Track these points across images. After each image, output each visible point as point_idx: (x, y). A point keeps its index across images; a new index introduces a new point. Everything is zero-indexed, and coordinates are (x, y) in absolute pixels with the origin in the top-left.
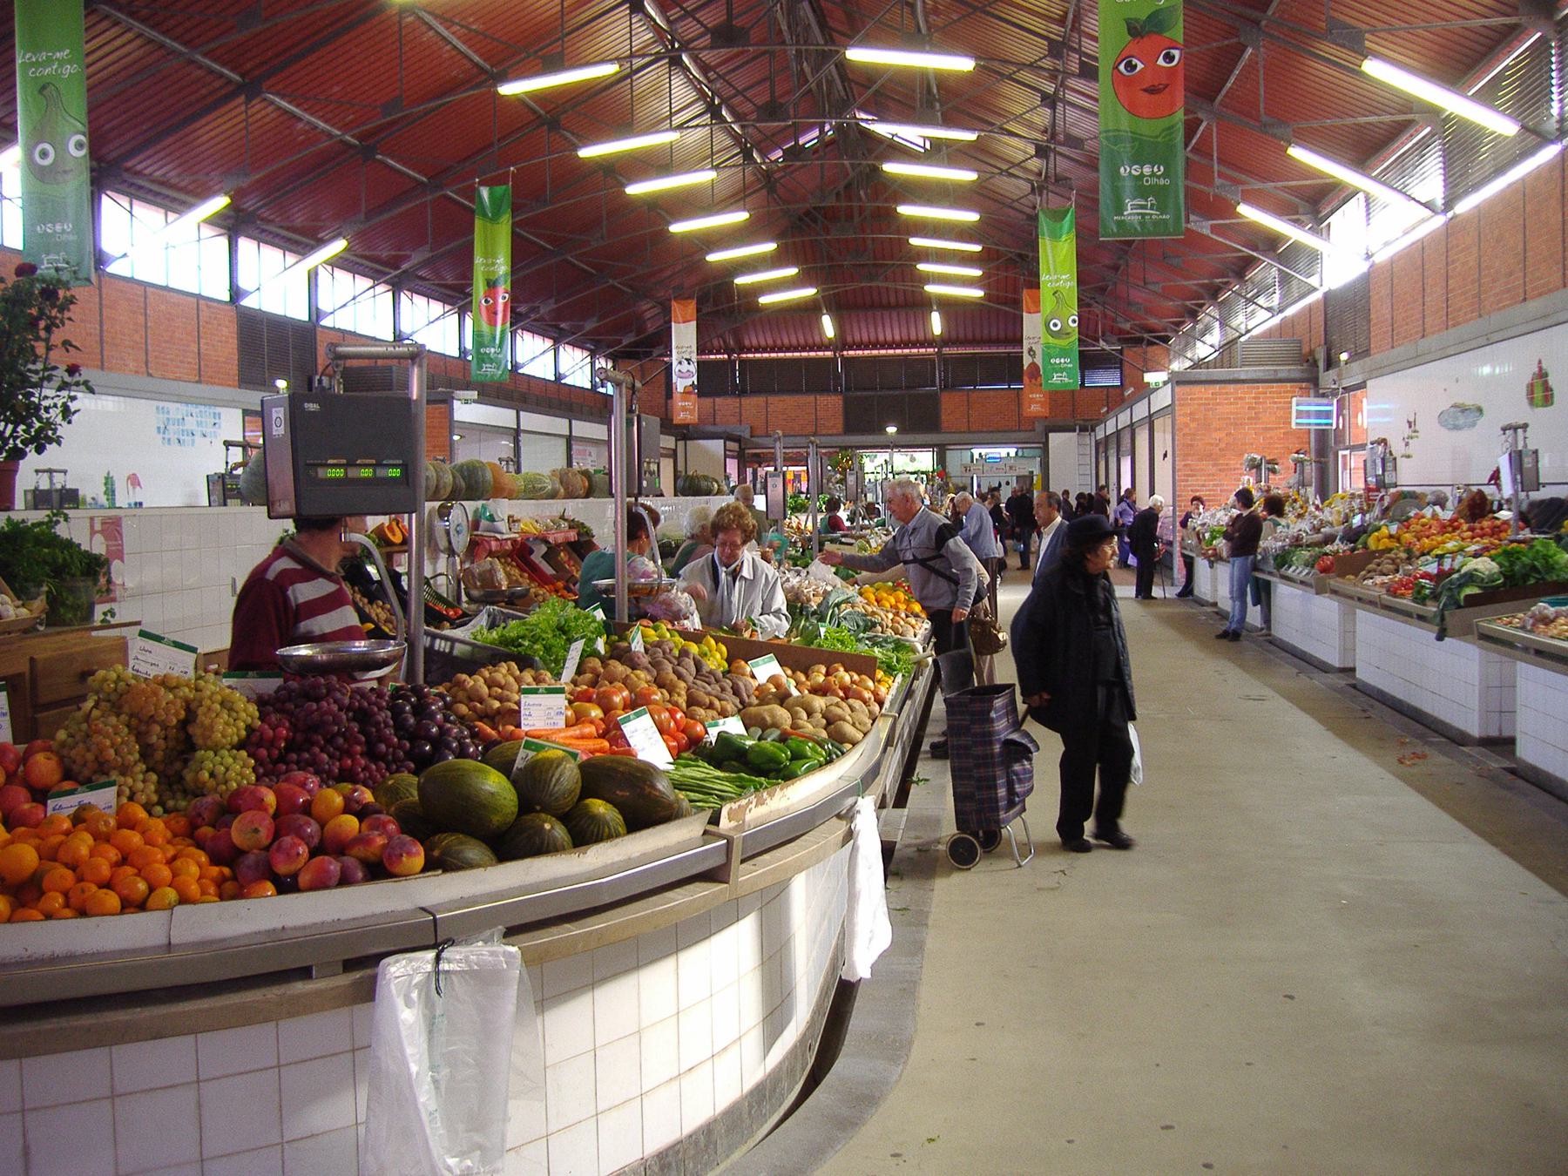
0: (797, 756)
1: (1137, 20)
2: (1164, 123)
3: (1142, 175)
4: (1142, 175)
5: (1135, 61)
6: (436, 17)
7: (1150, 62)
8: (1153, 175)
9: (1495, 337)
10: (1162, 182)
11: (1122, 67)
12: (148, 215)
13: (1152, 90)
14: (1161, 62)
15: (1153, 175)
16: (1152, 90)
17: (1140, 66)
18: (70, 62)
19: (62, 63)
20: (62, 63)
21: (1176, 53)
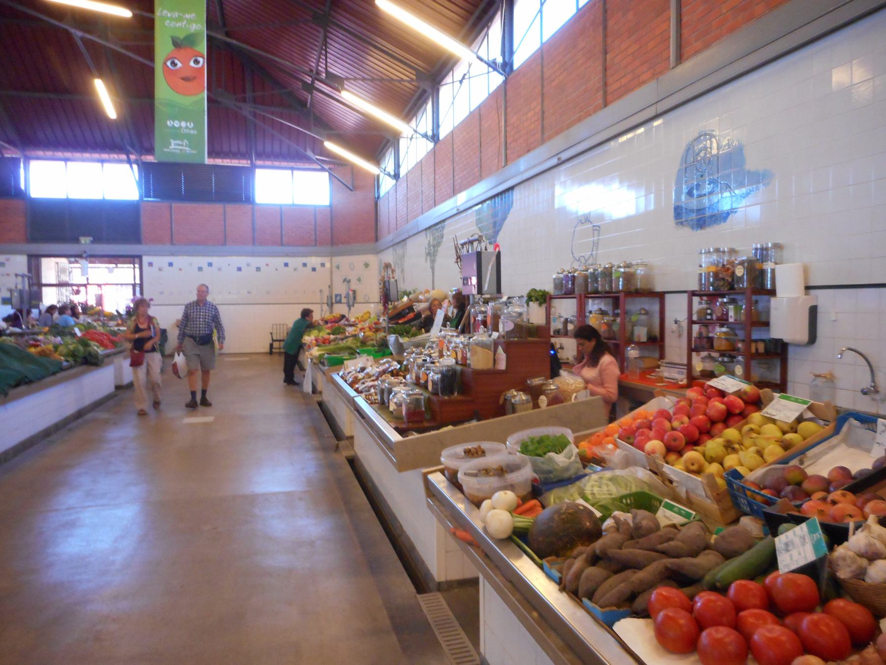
0: (590, 596)
1: (178, 38)
2: (198, 97)
3: (180, 127)
4: (180, 127)
5: (176, 61)
6: (492, 538)
7: (185, 63)
8: (187, 127)
9: (564, 156)
10: (192, 132)
11: (169, 63)
12: (493, 87)
13: (186, 79)
14: (192, 64)
15: (187, 127)
16: (186, 79)
17: (179, 65)
18: (195, 22)
19: (190, 21)
20: (190, 21)
21: (201, 60)
